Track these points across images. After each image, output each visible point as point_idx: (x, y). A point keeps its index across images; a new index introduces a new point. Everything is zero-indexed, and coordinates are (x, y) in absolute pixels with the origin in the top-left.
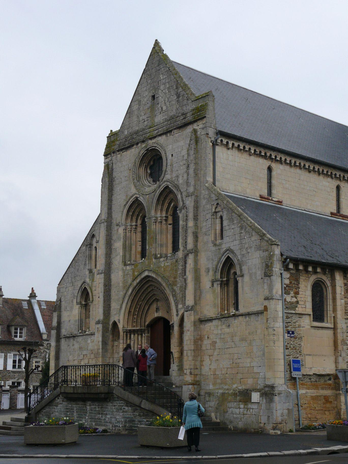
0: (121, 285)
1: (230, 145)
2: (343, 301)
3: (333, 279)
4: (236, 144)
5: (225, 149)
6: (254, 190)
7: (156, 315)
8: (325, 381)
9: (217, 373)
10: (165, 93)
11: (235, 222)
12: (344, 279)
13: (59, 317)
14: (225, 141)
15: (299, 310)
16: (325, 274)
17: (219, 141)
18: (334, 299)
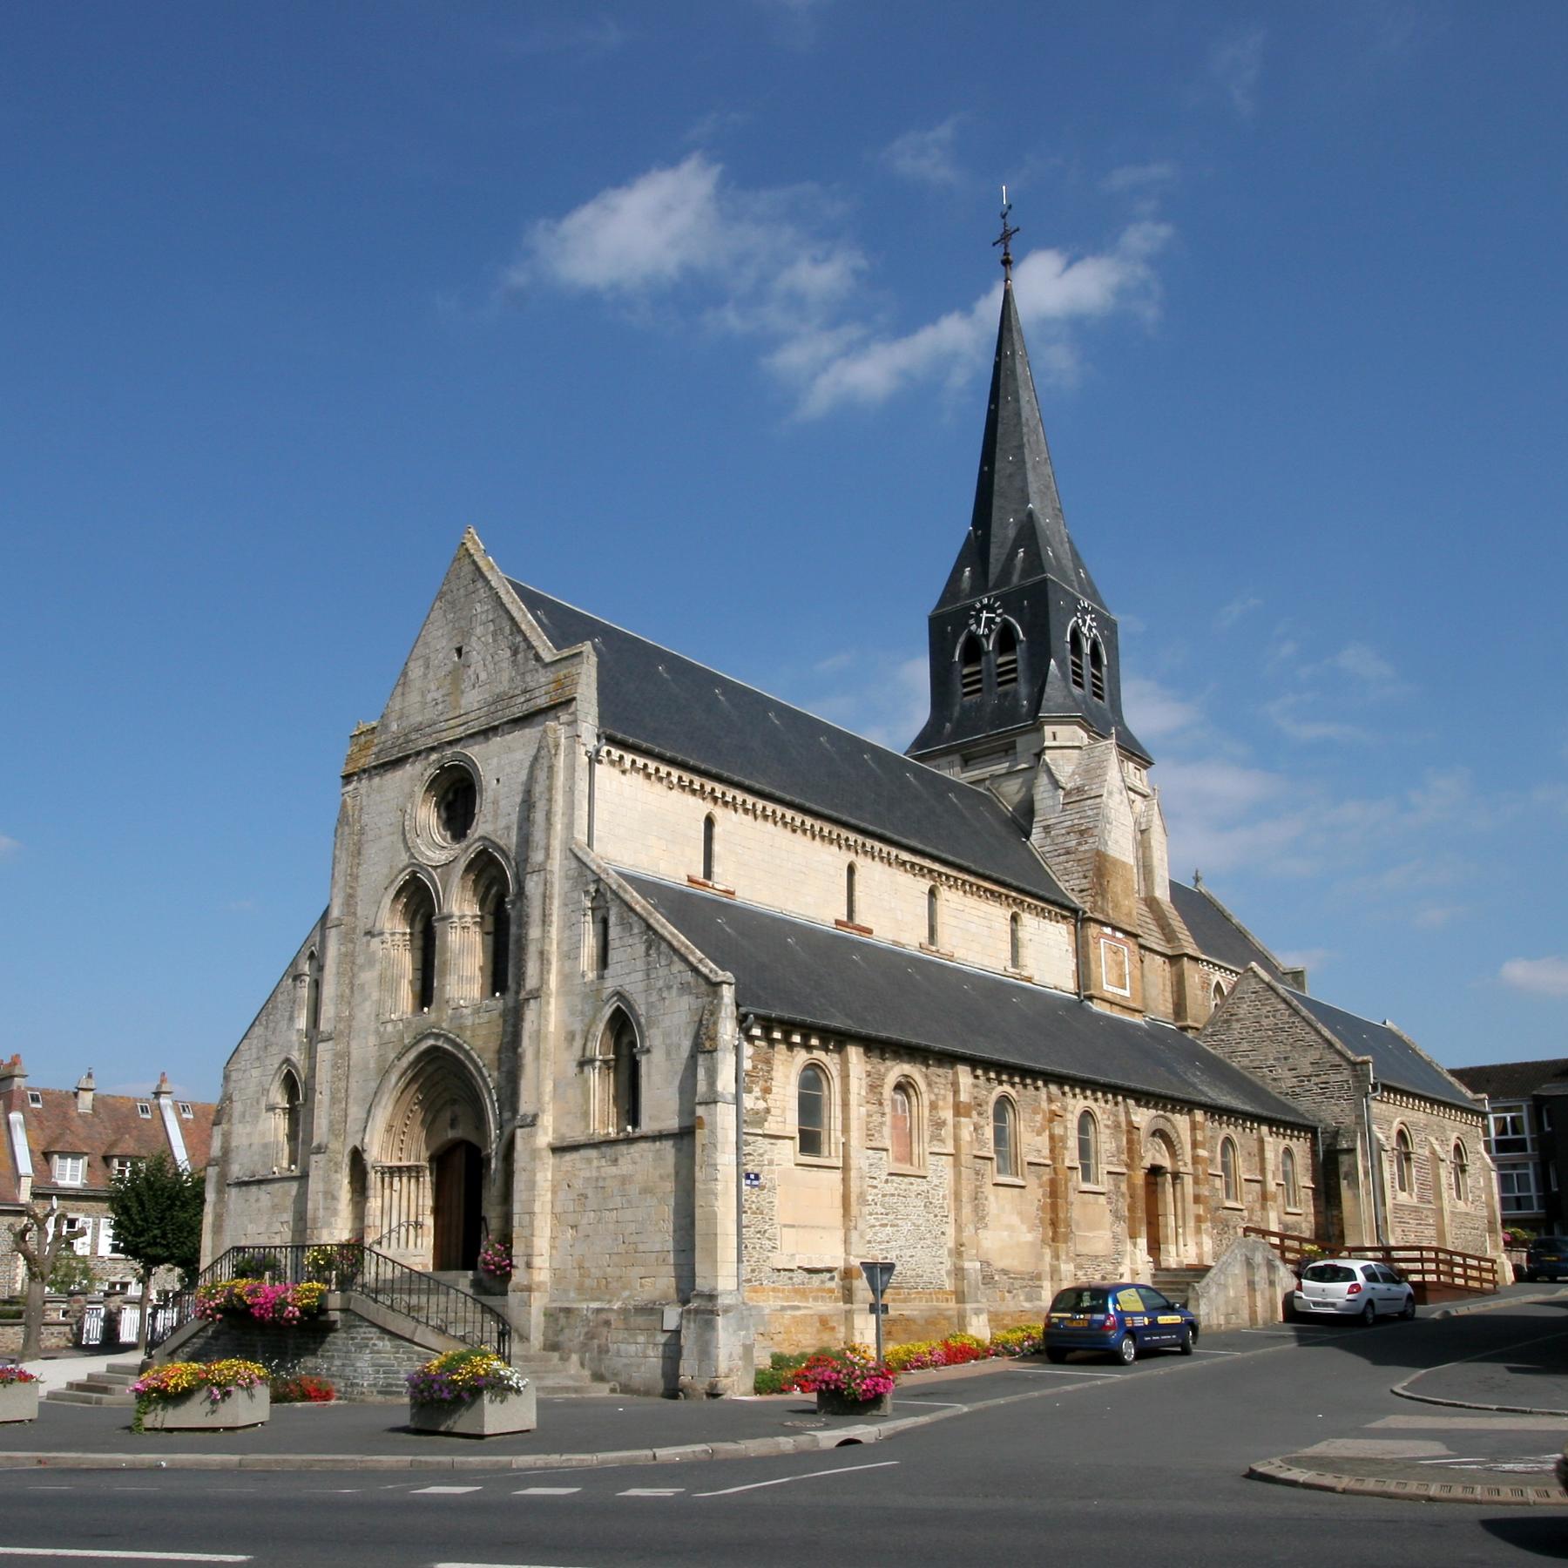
0: (372, 1065)
1: (628, 764)
2: (863, 1110)
3: (845, 1064)
4: (640, 762)
5: (616, 772)
6: (675, 864)
7: (451, 1134)
8: (823, 1282)
9: (586, 1265)
10: (486, 644)
11: (636, 931)
12: (866, 1053)
13: (227, 1136)
14: (616, 753)
15: (771, 1126)
16: (827, 1050)
17: (603, 753)
18: (845, 1104)
